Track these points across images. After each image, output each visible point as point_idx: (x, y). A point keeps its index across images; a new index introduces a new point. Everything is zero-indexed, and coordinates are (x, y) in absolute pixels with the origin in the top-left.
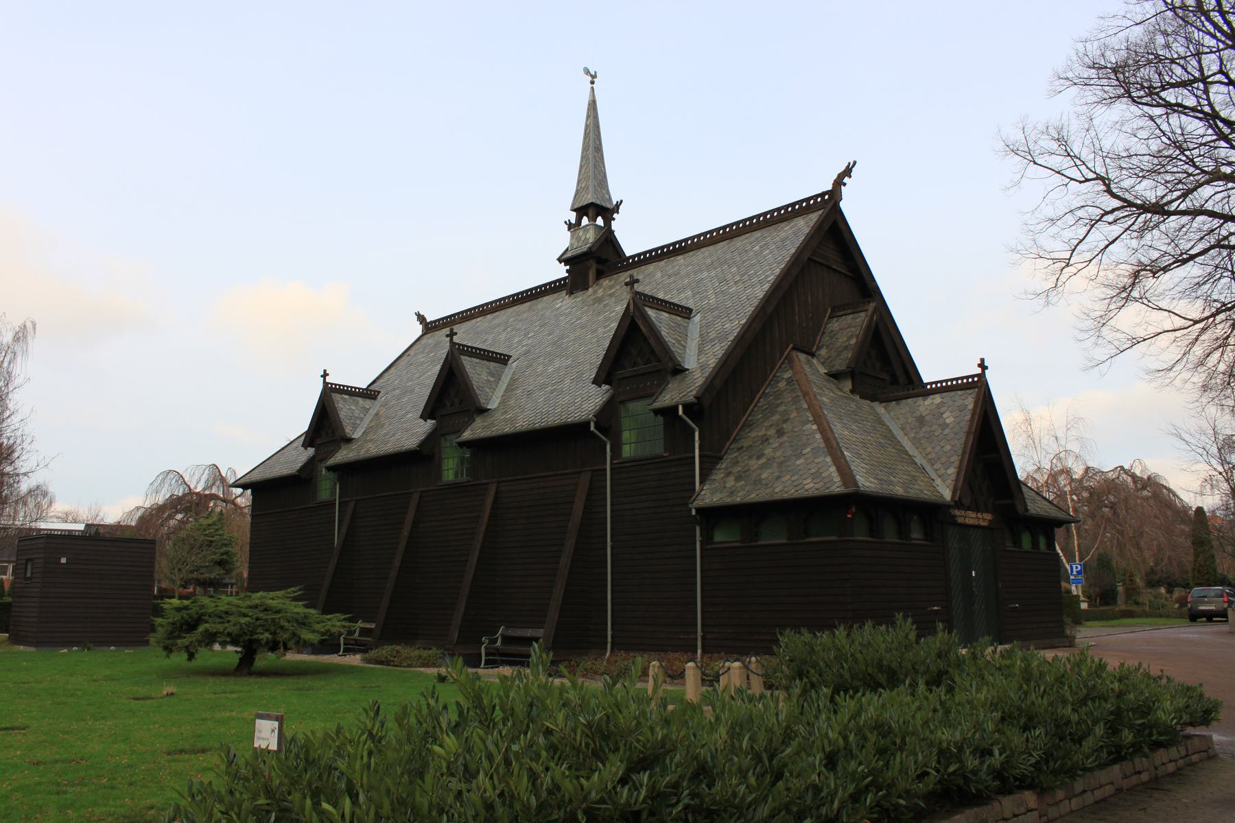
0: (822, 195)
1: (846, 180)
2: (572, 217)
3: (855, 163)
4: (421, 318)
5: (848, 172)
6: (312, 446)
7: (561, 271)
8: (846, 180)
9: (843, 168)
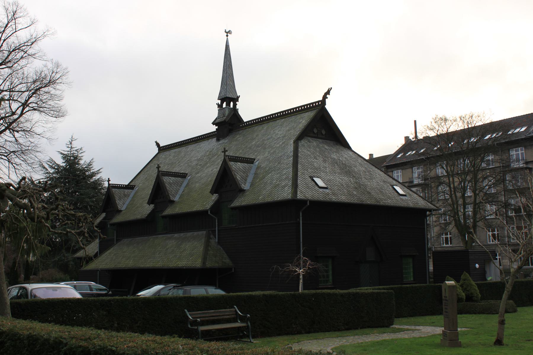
0: (318, 102)
1: (328, 96)
2: (219, 102)
3: (331, 88)
4: (158, 144)
5: (328, 92)
6: (216, 192)
7: (214, 128)
8: (328, 96)
9: (326, 91)
